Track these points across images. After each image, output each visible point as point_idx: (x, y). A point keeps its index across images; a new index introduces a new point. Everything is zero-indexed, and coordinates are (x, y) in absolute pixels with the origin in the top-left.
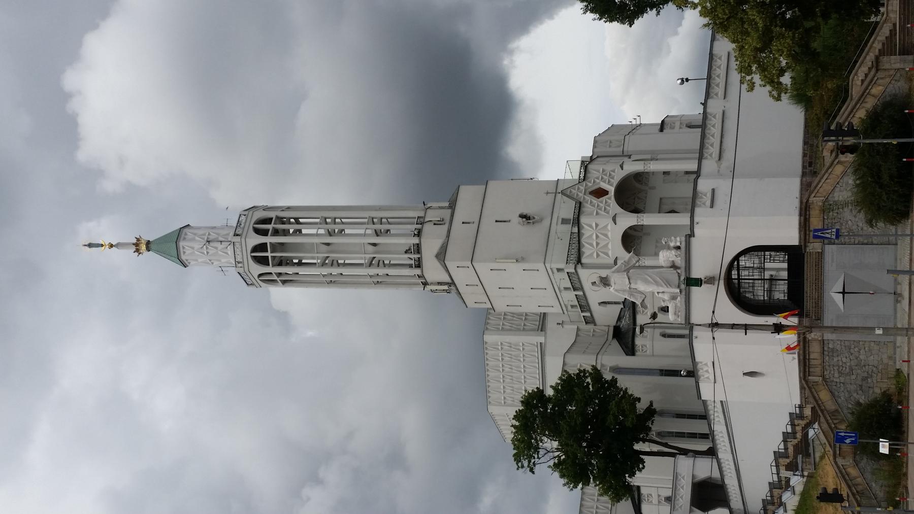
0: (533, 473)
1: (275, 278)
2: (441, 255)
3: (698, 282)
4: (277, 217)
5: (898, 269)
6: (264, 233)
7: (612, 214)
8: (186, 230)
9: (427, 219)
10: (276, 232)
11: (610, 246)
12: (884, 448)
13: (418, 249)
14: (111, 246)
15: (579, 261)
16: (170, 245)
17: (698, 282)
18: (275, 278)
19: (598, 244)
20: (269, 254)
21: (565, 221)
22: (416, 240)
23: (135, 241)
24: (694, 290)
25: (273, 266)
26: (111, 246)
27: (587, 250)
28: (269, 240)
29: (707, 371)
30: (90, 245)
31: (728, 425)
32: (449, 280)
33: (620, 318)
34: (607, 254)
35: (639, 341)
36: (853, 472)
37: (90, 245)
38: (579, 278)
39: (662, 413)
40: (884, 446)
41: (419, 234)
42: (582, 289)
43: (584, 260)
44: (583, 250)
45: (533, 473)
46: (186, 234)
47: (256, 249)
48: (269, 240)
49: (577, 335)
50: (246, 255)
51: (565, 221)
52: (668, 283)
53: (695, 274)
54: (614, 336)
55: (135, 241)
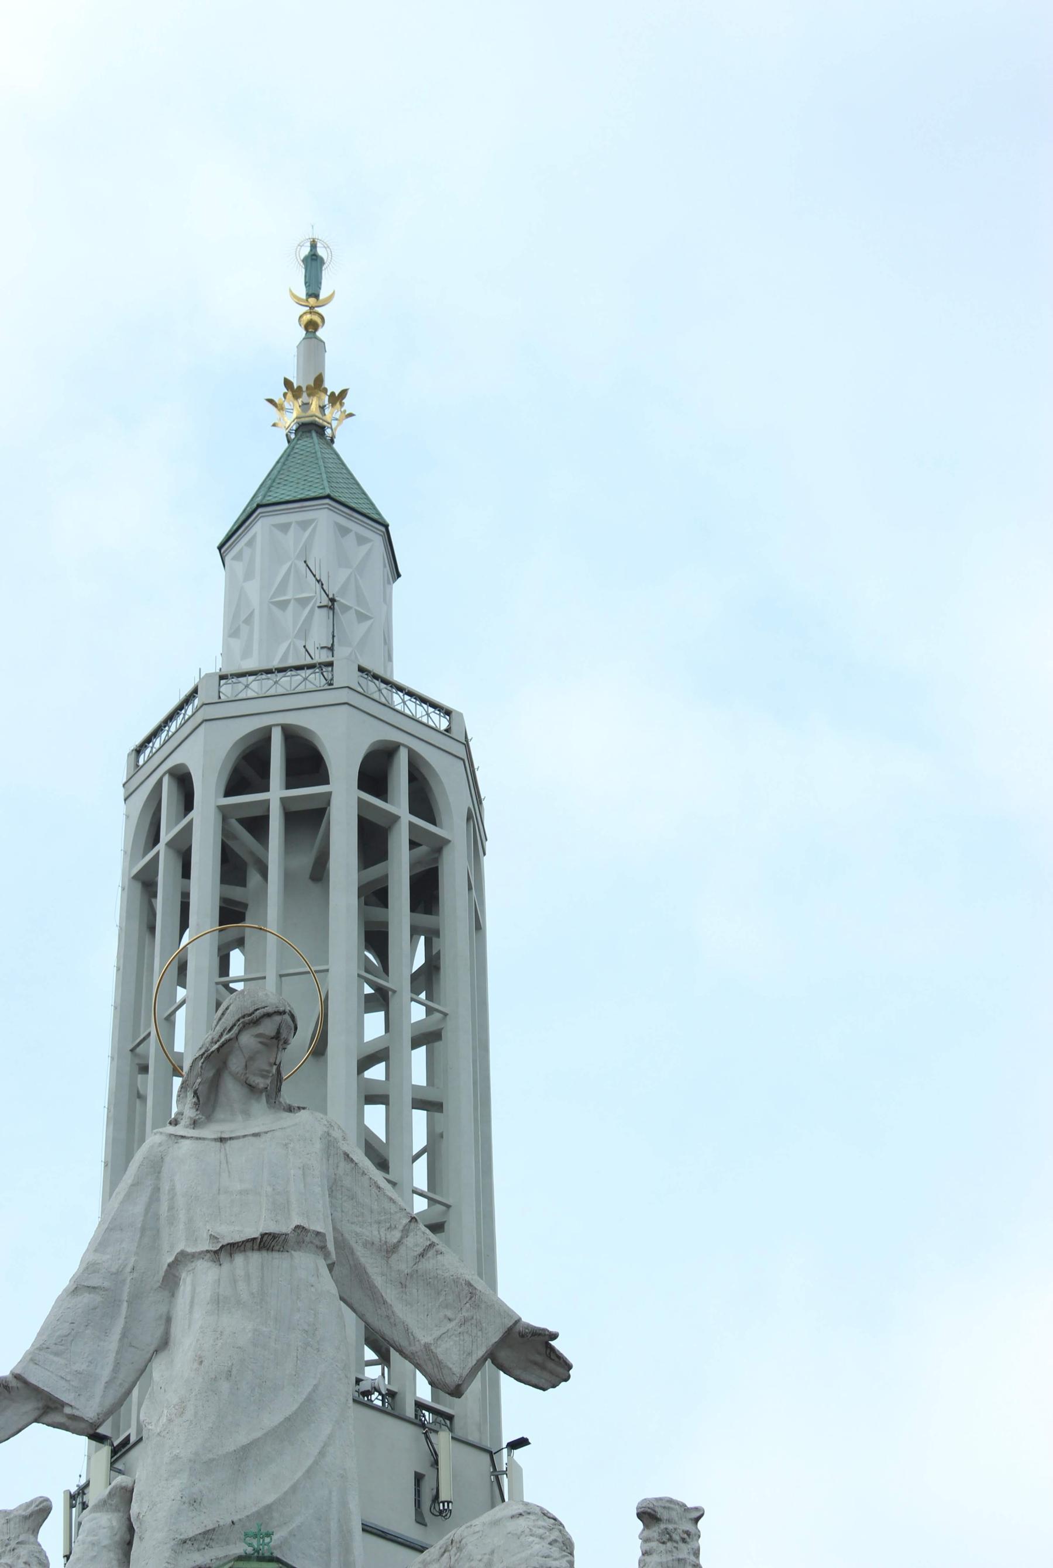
0: (344, 393)
4: (439, 846)
6: (374, 774)
8: (378, 542)
9: (443, 1440)
10: (373, 840)
14: (311, 327)
16: (310, 481)
20: (277, 793)
23: (332, 385)
25: (225, 813)
26: (311, 327)
28: (343, 796)
30: (313, 263)
31: (423, 700)
37: (313, 263)
45: (344, 393)
46: (361, 540)
48: (343, 796)
50: (273, 708)
55: (332, 385)
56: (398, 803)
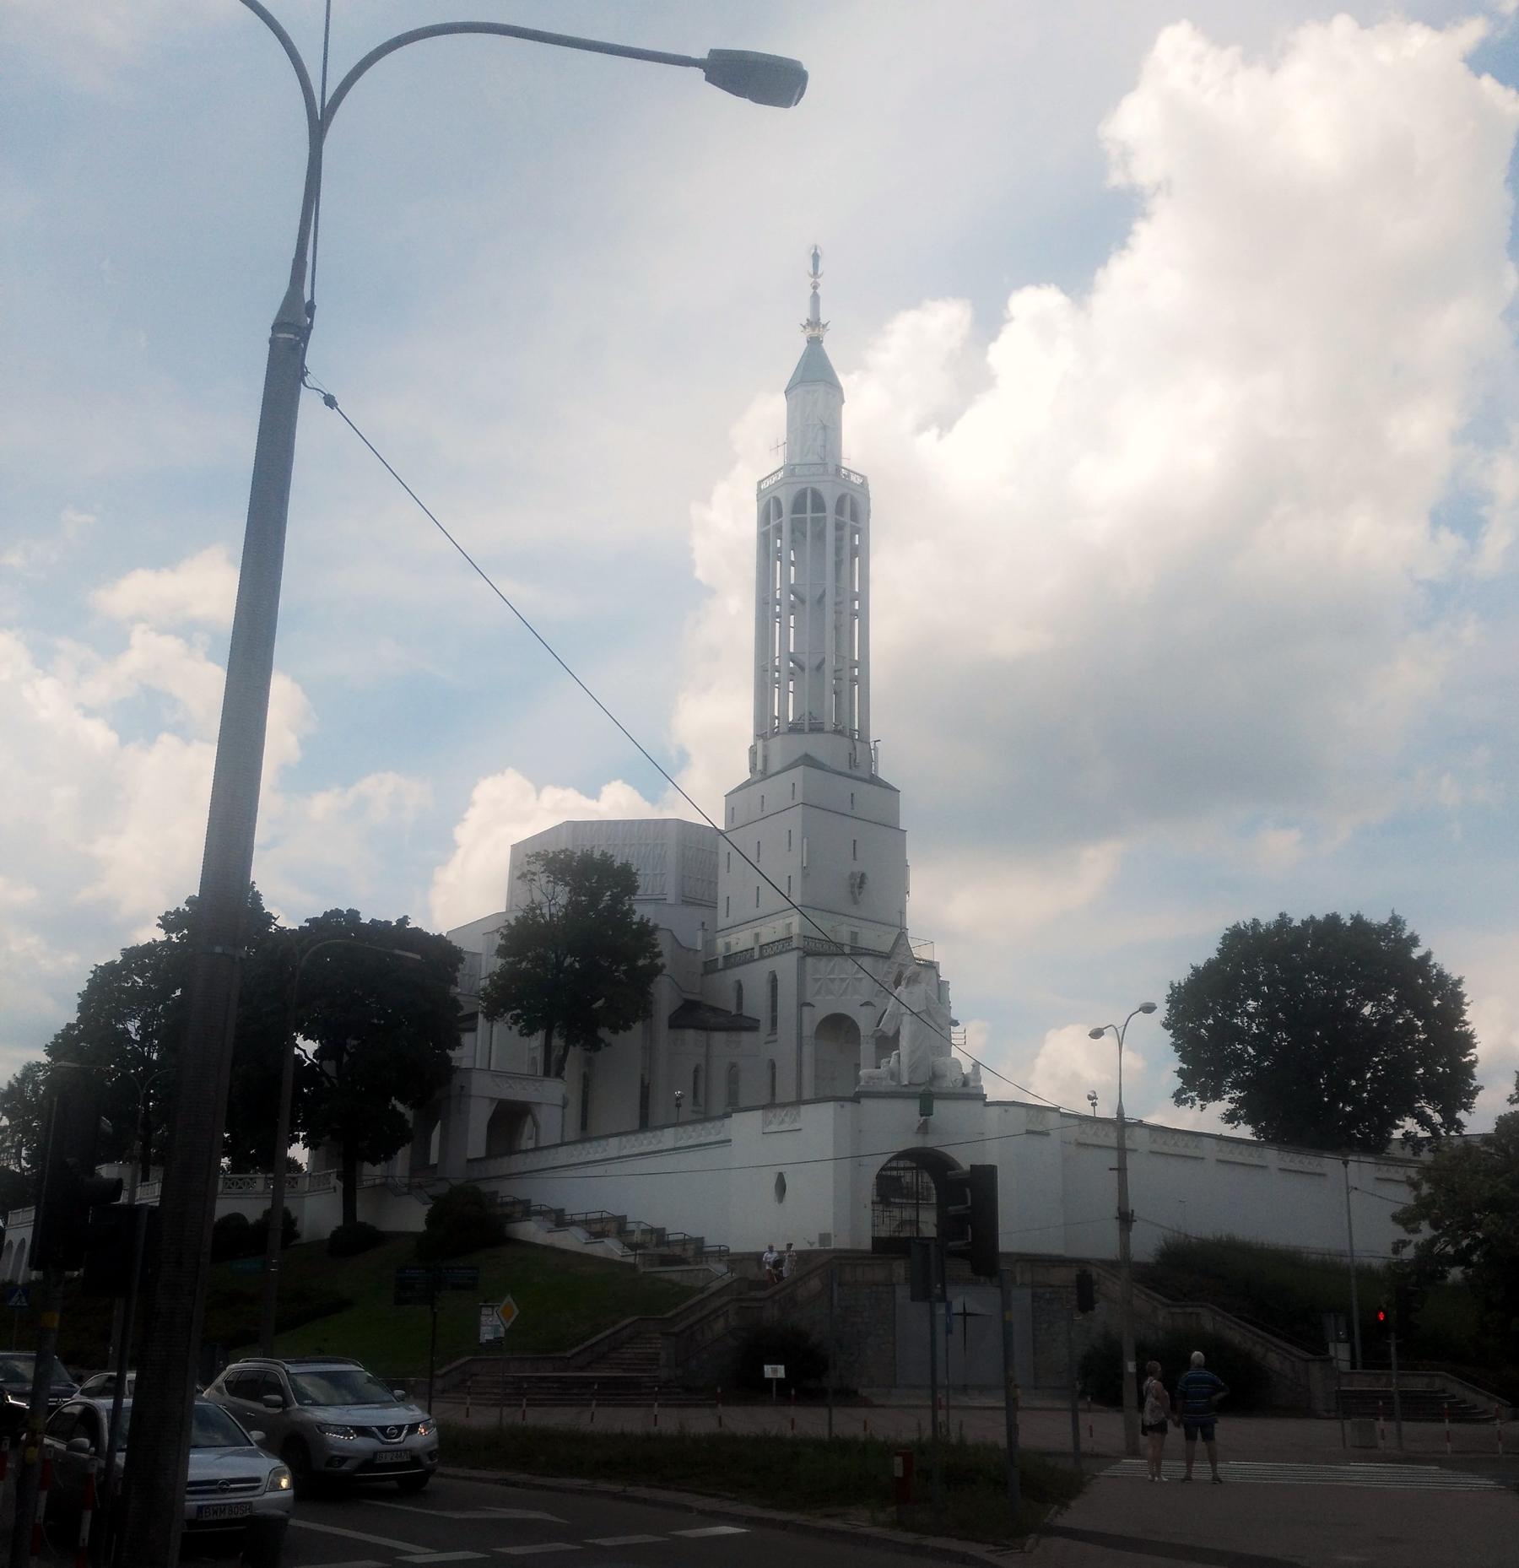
1: (773, 523)
2: (808, 761)
3: (926, 1111)
5: (1020, 1416)
6: (839, 510)
7: (876, 1001)
11: (830, 997)
12: (774, 1371)
13: (817, 728)
14: (815, 288)
15: (807, 953)
17: (926, 1111)
18: (773, 523)
19: (832, 980)
20: (809, 515)
21: (854, 935)
22: (828, 727)
23: (823, 321)
24: (914, 1106)
26: (815, 288)
27: (824, 965)
28: (830, 516)
29: (783, 1122)
30: (816, 258)
32: (770, 772)
33: (714, 1010)
34: (818, 993)
35: (690, 1035)
36: (719, 1325)
38: (781, 953)
39: (589, 1062)
40: (775, 1371)
41: (838, 732)
42: (762, 957)
43: (809, 960)
44: (825, 959)
47: (816, 495)
48: (830, 516)
49: (689, 950)
51: (854, 935)
52: (913, 1069)
53: (939, 1107)
54: (687, 1001)
56: (847, 518)
